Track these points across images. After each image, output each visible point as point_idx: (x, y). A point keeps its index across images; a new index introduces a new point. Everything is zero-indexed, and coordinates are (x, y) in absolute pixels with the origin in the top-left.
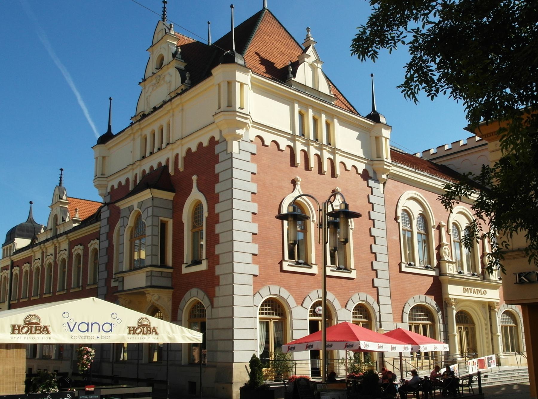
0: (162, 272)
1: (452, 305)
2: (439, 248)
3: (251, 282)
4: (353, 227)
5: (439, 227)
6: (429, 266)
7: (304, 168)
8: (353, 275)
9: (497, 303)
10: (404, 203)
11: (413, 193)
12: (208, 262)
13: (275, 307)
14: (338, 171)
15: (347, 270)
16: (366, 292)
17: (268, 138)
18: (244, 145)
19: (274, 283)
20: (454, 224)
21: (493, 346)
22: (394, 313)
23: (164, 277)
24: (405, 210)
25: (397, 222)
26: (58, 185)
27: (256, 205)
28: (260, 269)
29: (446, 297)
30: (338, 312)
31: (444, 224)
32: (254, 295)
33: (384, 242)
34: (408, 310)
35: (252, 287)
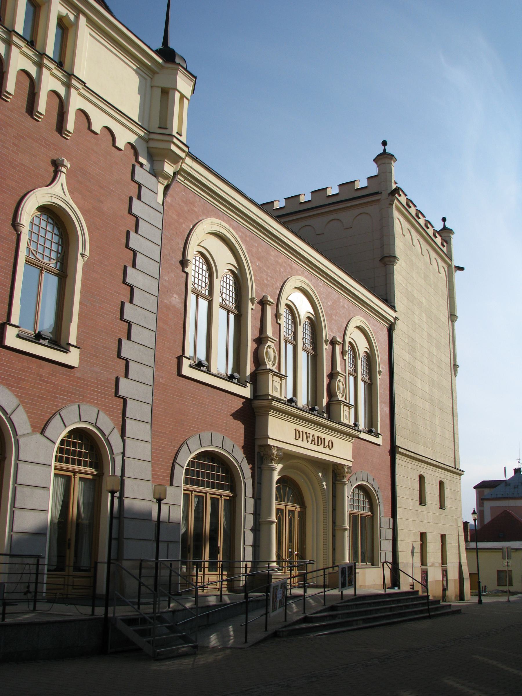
1: (272, 460)
2: (333, 375)
4: (87, 253)
5: (263, 303)
6: (236, 375)
7: (55, 129)
8: (72, 358)
9: (349, 467)
10: (202, 238)
11: (302, 281)
14: (70, 125)
15: (59, 346)
16: (97, 405)
20: (350, 343)
21: (334, 549)
22: (155, 461)
24: (287, 305)
25: (183, 271)
29: (263, 443)
30: (22, 441)
31: (272, 300)
33: (151, 303)
34: (186, 458)
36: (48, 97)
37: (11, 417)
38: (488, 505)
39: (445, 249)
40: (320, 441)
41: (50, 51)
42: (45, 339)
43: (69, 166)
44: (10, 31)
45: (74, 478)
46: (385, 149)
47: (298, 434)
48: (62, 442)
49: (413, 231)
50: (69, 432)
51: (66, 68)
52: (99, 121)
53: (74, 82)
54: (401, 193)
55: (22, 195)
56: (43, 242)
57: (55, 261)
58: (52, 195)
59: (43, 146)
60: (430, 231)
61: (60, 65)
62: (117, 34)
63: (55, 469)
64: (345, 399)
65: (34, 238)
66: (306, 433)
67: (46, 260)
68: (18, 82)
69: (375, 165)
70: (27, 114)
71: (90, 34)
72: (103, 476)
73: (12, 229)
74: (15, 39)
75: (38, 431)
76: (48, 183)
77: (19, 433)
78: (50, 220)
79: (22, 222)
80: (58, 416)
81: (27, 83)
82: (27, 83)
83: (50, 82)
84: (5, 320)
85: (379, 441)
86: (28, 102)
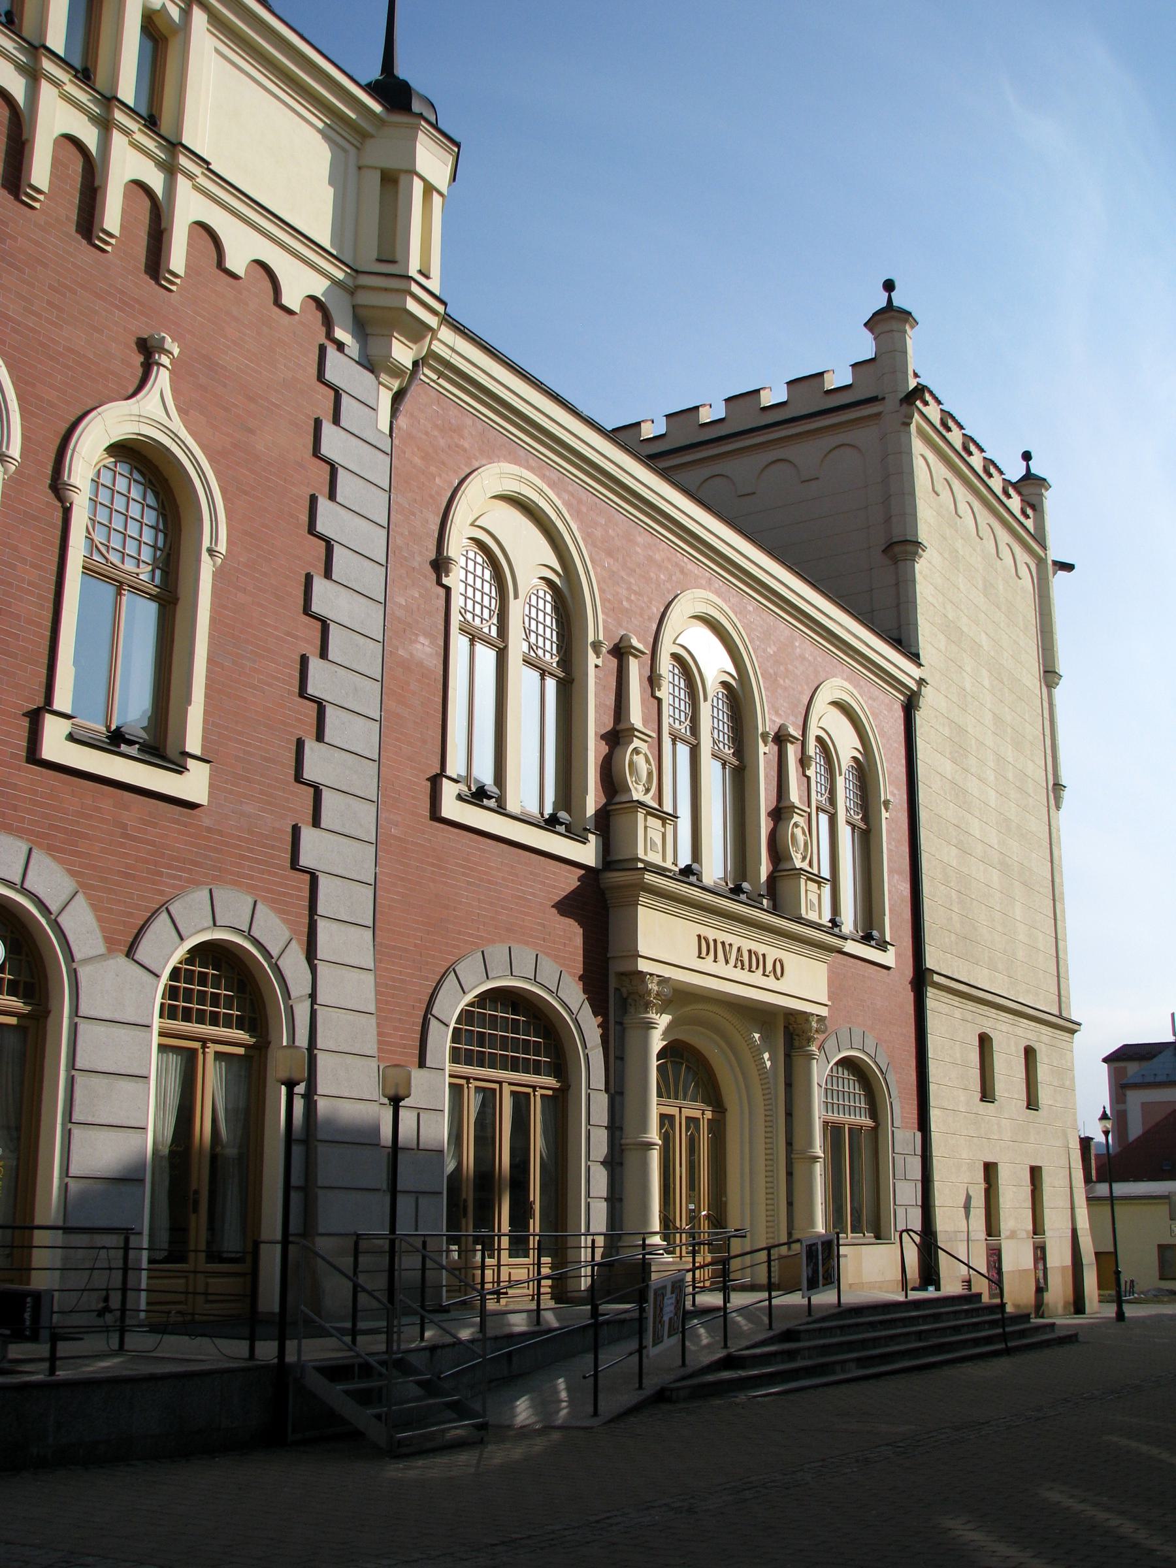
4: (222, 547)
36: (126, 196)
37: (60, 919)
38: (1136, 1099)
39: (1029, 524)
40: (754, 961)
41: (127, 89)
42: (131, 743)
43: (176, 351)
44: (36, 48)
45: (204, 1053)
46: (890, 300)
47: (705, 947)
48: (175, 974)
49: (957, 484)
50: (189, 951)
52: (242, 248)
53: (184, 161)
54: (928, 397)
57: (150, 568)
59: (117, 307)
60: (996, 484)
61: (151, 122)
62: (256, 32)
63: (161, 1034)
64: (811, 865)
66: (723, 943)
67: (129, 566)
69: (869, 336)
71: (217, 51)
73: (52, 496)
74: (47, 65)
75: (121, 951)
76: (131, 391)
77: (78, 956)
78: (137, 476)
79: (72, 481)
80: (164, 915)
82: (76, 165)
83: (129, 162)
84: (40, 702)
85: (888, 958)
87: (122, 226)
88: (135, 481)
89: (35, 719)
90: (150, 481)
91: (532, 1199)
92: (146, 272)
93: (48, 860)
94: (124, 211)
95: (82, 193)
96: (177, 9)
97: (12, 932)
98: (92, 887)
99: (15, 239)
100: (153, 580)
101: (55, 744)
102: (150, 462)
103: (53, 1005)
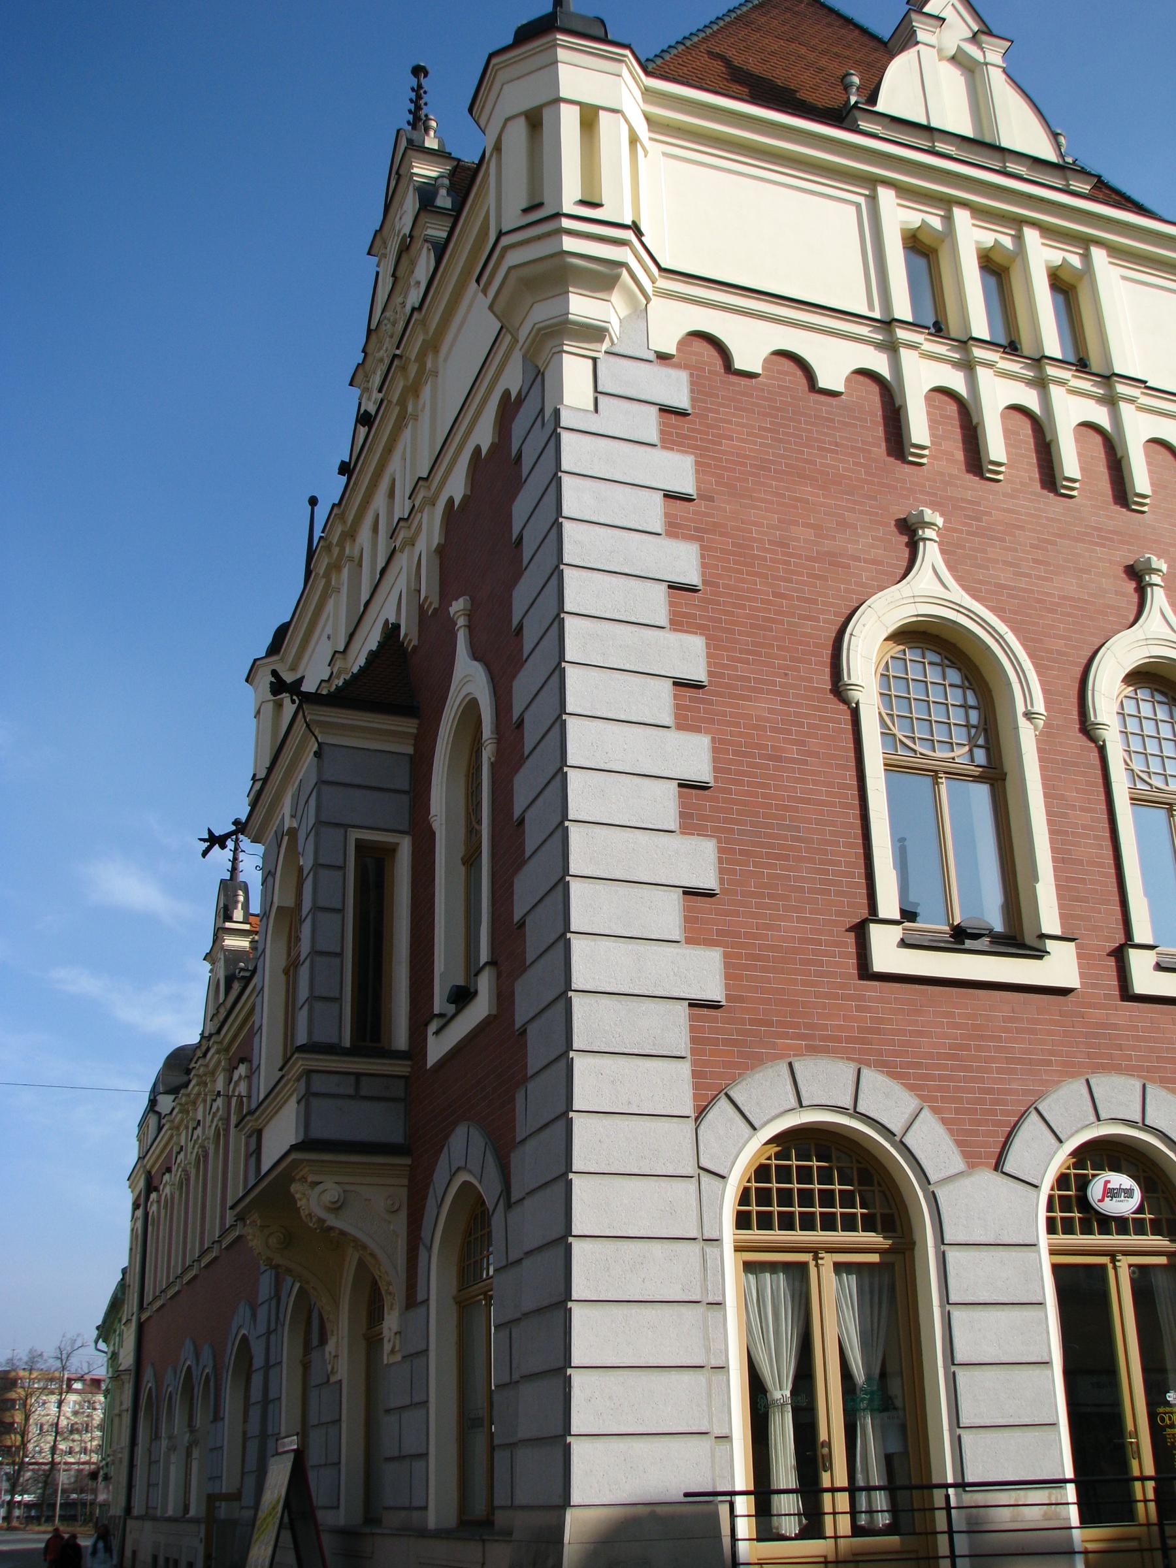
0: (358, 1076)
3: (679, 1041)
4: (1039, 706)
12: (499, 976)
13: (832, 1181)
14: (1141, 479)
17: (751, 345)
18: (615, 375)
19: (820, 1045)
23: (365, 1098)
26: (227, 876)
27: (696, 644)
28: (731, 974)
32: (701, 1113)
35: (684, 1069)
36: (1147, 456)
37: (907, 1140)
41: (1053, 346)
42: (976, 937)
43: (1164, 568)
44: (965, 343)
45: (1115, 1268)
50: (1074, 1154)
51: (1095, 368)
53: (1121, 389)
55: (1085, 661)
56: (1157, 747)
57: (967, 748)
58: (915, 599)
59: (1097, 544)
61: (1082, 365)
62: (1009, 203)
63: (1052, 1253)
65: (1136, 744)
67: (942, 753)
68: (1008, 433)
70: (1045, 492)
71: (1124, 278)
72: (913, 1249)
73: (1084, 738)
74: (978, 353)
75: (987, 1165)
76: (1132, 618)
77: (933, 1179)
78: (1158, 697)
79: (1099, 720)
80: (1034, 1116)
81: (952, 408)
82: (1025, 429)
83: (1072, 408)
84: (1120, 938)
86: (1040, 467)
87: (1082, 469)
88: (1159, 702)
89: (860, 932)
90: (1173, 698)
91: (823, 1436)
92: (1116, 503)
93: (1163, 1093)
94: (1079, 455)
95: (1037, 452)
96: (1009, 238)
97: (1144, 1171)
98: (935, 1099)
99: (989, 514)
100: (973, 761)
101: (887, 951)
102: (1162, 677)
103: (917, 1237)
